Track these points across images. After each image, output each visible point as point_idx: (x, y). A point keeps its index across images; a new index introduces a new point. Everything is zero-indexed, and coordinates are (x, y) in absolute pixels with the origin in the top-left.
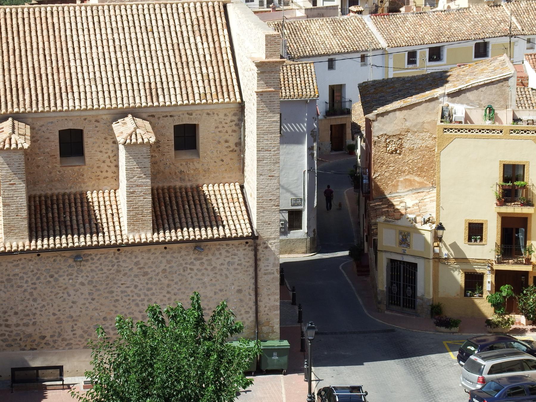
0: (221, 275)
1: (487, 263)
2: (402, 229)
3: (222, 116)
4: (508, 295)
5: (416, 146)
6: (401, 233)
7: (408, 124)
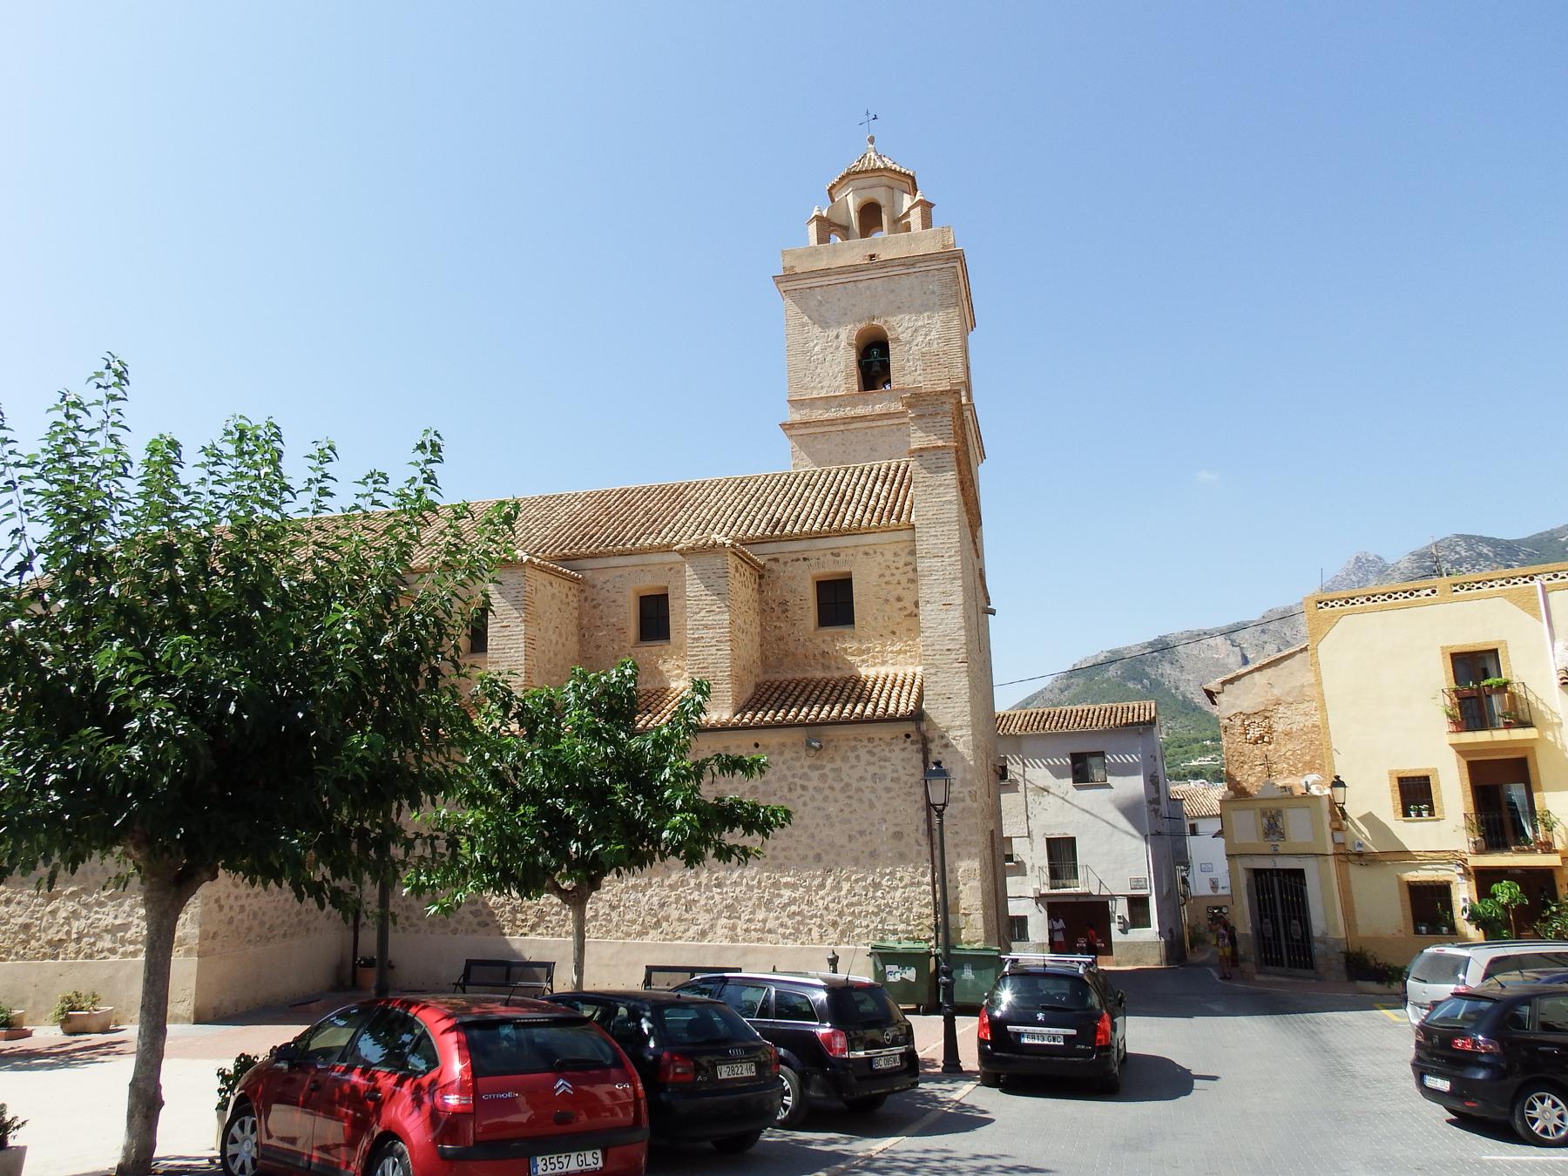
0: (860, 800)
1: (1454, 858)
2: (1265, 805)
3: (889, 556)
4: (1512, 900)
5: (1295, 727)
6: (1264, 814)
7: (1277, 692)
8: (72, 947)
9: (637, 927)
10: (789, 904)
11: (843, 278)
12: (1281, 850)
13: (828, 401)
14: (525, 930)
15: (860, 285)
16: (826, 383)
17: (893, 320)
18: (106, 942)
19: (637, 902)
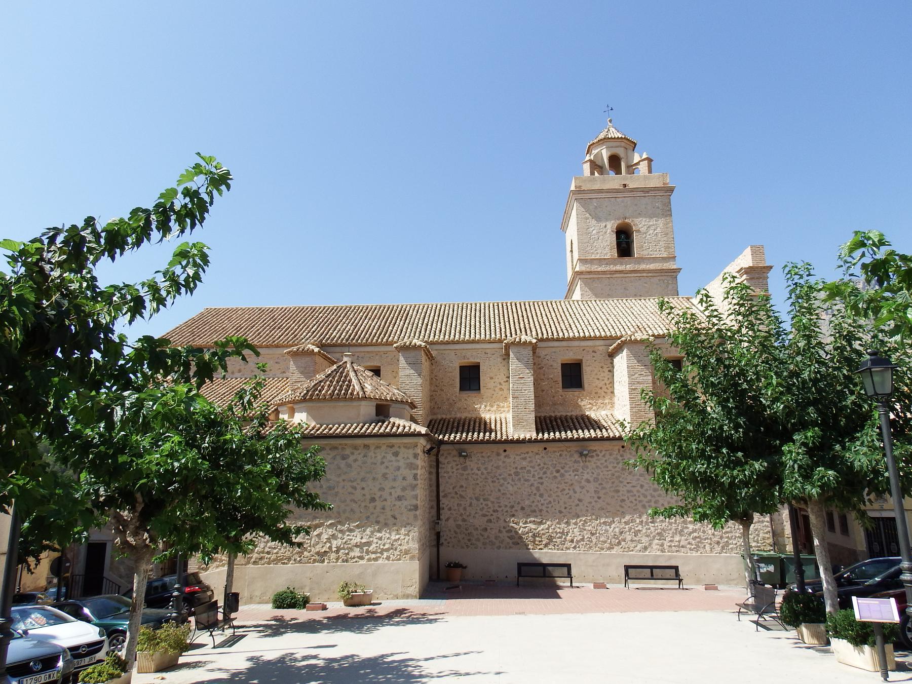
8: (333, 556)
9: (607, 545)
10: (692, 532)
11: (609, 195)
12: (885, 507)
13: (600, 261)
14: (541, 547)
15: (618, 200)
16: (599, 251)
17: (637, 221)
18: (356, 552)
19: (607, 531)
